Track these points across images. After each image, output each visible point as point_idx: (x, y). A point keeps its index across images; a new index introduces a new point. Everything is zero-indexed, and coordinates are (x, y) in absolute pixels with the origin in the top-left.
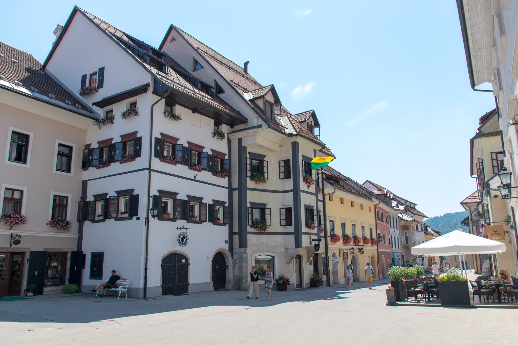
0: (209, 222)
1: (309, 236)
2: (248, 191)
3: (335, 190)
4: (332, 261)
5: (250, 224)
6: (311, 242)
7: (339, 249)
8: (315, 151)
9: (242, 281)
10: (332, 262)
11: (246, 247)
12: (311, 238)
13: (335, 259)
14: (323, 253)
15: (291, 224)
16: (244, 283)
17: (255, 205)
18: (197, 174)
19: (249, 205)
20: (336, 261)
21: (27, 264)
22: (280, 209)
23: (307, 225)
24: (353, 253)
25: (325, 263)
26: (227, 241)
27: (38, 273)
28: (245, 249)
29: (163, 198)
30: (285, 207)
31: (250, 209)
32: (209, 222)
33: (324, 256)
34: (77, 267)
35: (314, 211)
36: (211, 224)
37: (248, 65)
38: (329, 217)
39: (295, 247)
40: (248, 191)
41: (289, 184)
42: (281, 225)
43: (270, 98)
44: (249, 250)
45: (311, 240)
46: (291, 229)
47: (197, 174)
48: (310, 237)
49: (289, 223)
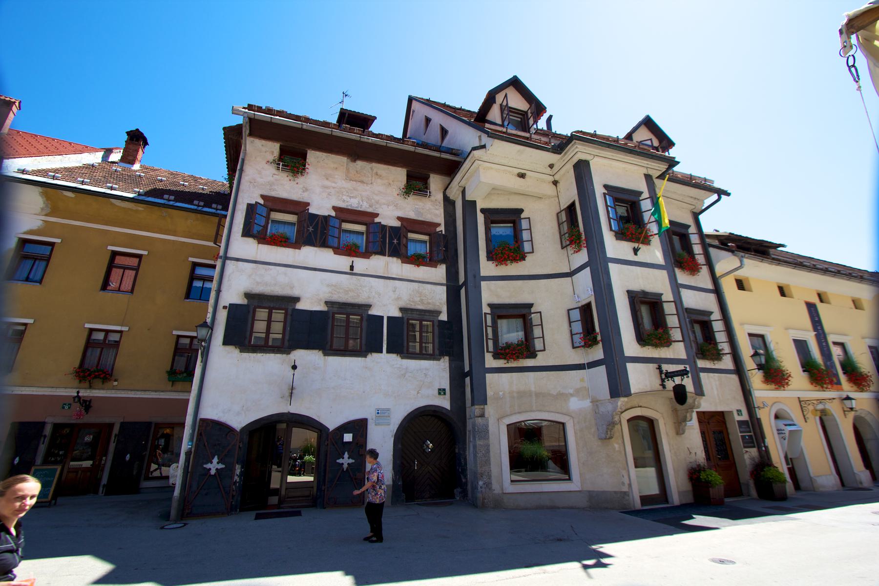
0: (388, 352)
1: (656, 366)
2: (483, 283)
3: (741, 261)
4: (778, 430)
5: (491, 348)
6: (663, 380)
7: (800, 402)
8: (648, 177)
9: (477, 483)
10: (779, 434)
11: (485, 402)
12: (661, 372)
13: (786, 425)
14: (739, 412)
15: (595, 342)
16: (481, 487)
17: (501, 311)
18: (353, 261)
19: (486, 309)
20: (790, 431)
21: (114, 442)
22: (569, 310)
23: (642, 339)
24: (852, 409)
25: (750, 436)
26: (444, 390)
27: (19, 461)
28: (482, 407)
29: (274, 311)
30: (580, 305)
31: (489, 318)
32: (388, 352)
33: (745, 417)
34: (20, 459)
35: (713, 323)
36: (393, 357)
37: (552, 121)
38: (742, 324)
39: (611, 398)
40: (483, 283)
41: (582, 257)
42: (574, 347)
43: (516, 102)
44: (490, 410)
45: (663, 376)
46: (597, 353)
47: (353, 261)
48: (660, 368)
49: (589, 338)
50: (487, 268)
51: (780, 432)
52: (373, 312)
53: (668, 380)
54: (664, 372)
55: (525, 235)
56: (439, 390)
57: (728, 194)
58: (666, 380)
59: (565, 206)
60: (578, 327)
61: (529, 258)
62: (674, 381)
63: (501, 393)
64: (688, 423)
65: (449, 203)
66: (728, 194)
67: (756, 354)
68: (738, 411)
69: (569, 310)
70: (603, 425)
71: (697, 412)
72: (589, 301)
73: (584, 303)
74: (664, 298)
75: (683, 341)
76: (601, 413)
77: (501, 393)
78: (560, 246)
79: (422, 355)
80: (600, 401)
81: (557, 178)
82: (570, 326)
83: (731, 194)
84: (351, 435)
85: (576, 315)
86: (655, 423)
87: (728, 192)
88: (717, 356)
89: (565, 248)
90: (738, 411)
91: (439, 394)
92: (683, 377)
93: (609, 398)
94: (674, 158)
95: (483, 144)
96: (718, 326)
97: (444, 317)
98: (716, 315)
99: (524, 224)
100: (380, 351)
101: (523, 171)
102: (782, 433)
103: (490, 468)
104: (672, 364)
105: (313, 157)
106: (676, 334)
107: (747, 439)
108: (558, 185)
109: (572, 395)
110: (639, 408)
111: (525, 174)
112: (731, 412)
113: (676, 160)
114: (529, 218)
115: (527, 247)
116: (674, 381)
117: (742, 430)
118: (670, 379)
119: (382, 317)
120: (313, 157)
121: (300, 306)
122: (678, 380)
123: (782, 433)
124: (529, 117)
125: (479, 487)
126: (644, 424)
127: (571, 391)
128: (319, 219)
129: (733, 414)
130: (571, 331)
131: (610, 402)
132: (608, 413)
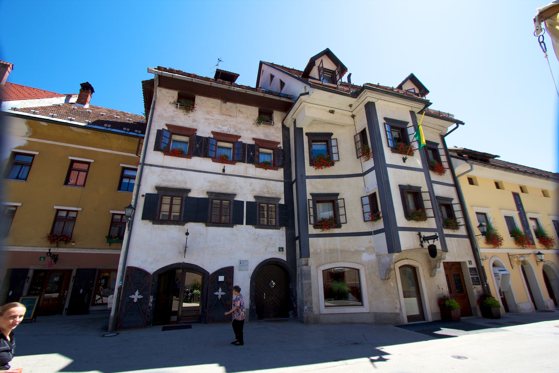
0: (247, 224)
1: (417, 233)
2: (307, 180)
3: (471, 166)
4: (495, 274)
5: (312, 222)
6: (421, 242)
7: (509, 256)
8: (412, 113)
9: (304, 307)
10: (495, 276)
11: (308, 256)
12: (420, 237)
13: (500, 271)
14: (470, 262)
15: (378, 218)
16: (306, 310)
17: (319, 198)
18: (224, 166)
19: (309, 197)
20: (503, 274)
21: (73, 282)
22: (362, 198)
23: (408, 216)
24: (542, 260)
25: (477, 278)
26: (282, 248)
27: (12, 294)
28: (307, 259)
29: (174, 198)
30: (369, 194)
31: (311, 202)
32: (247, 224)
33: (474, 265)
35: (453, 205)
36: (250, 227)
37: (351, 77)
38: (472, 206)
39: (389, 253)
40: (307, 180)
41: (370, 164)
42: (365, 221)
43: (328, 65)
44: (312, 261)
45: (422, 239)
46: (380, 224)
47: (224, 166)
48: (419, 234)
49: (374, 215)
50: (310, 170)
51: (496, 275)
52: (237, 198)
53: (425, 242)
54: (423, 236)
55: (334, 150)
56: (279, 248)
57: (463, 124)
58: (423, 242)
59: (360, 131)
60: (368, 208)
61: (336, 164)
62: (428, 243)
63: (318, 250)
64: (438, 269)
65: (285, 129)
66: (463, 124)
67: (481, 226)
68: (469, 261)
69: (362, 198)
70: (383, 270)
71: (443, 262)
72: (375, 191)
73: (371, 193)
74: (422, 190)
75: (434, 217)
76: (382, 263)
77: (318, 250)
78: (356, 157)
79: (268, 226)
80: (382, 255)
81: (354, 113)
82: (363, 208)
83: (465, 124)
84: (223, 277)
85: (366, 200)
86: (417, 269)
87: (463, 122)
88: (456, 226)
89: (360, 158)
90: (469, 261)
91: (279, 251)
92: (434, 240)
93: (388, 253)
94: (429, 100)
95: (307, 91)
96: (457, 208)
97: (282, 202)
98: (456, 201)
99: (333, 143)
100: (242, 223)
101: (333, 109)
102: (497, 276)
103: (312, 298)
104: (427, 231)
105: (199, 100)
106: (430, 213)
107: (475, 280)
108: (355, 117)
109: (364, 251)
110: (407, 260)
111: (334, 111)
112: (465, 262)
113: (430, 102)
114: (336, 139)
115: (335, 157)
116: (428, 243)
117: (472, 274)
118: (426, 241)
119: (243, 202)
120: (199, 100)
121: (191, 195)
122: (431, 242)
123: (497, 276)
124: (337, 75)
125: (305, 310)
126: (410, 270)
127: (363, 249)
128: (203, 139)
129: (466, 263)
130: (363, 211)
131: (388, 256)
132: (387, 263)
